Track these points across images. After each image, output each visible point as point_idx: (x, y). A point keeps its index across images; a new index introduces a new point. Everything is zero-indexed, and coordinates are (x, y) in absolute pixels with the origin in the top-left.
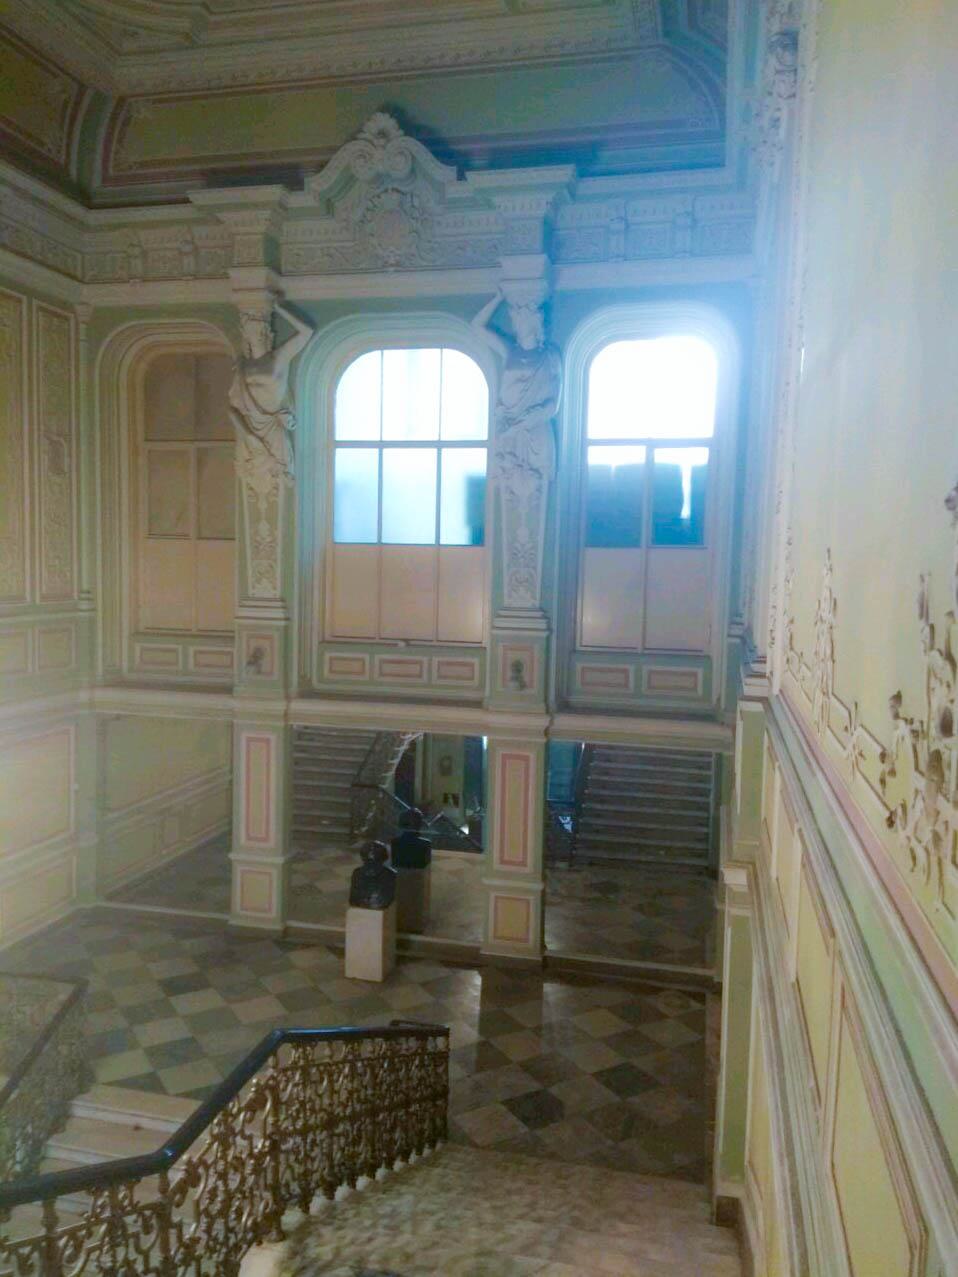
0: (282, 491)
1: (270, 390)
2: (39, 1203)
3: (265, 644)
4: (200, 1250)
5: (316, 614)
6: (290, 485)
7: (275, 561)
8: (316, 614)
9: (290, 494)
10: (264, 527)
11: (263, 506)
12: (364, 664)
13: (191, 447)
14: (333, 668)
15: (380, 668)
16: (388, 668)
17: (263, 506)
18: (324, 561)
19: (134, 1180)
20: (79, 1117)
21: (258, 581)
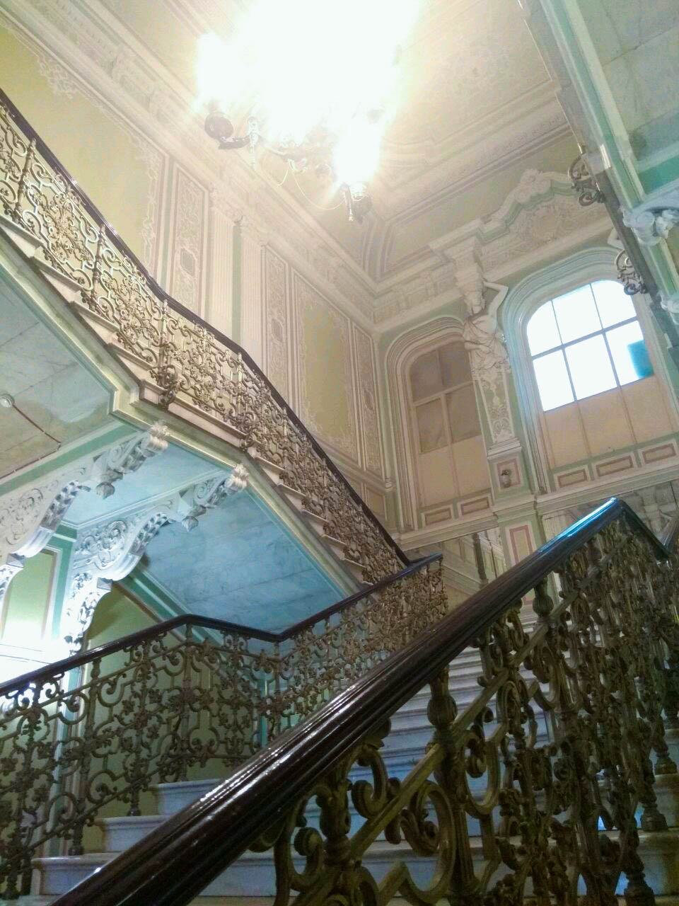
0: (504, 377)
1: (488, 323)
2: (585, 894)
3: (511, 466)
4: (238, 733)
5: (542, 457)
6: (509, 371)
7: (507, 416)
8: (542, 457)
9: (510, 376)
10: (496, 400)
11: (493, 388)
12: (585, 473)
13: (441, 395)
14: (563, 484)
15: (598, 471)
16: (603, 470)
17: (493, 388)
18: (539, 421)
19: (162, 635)
20: (200, 682)
21: (498, 432)
